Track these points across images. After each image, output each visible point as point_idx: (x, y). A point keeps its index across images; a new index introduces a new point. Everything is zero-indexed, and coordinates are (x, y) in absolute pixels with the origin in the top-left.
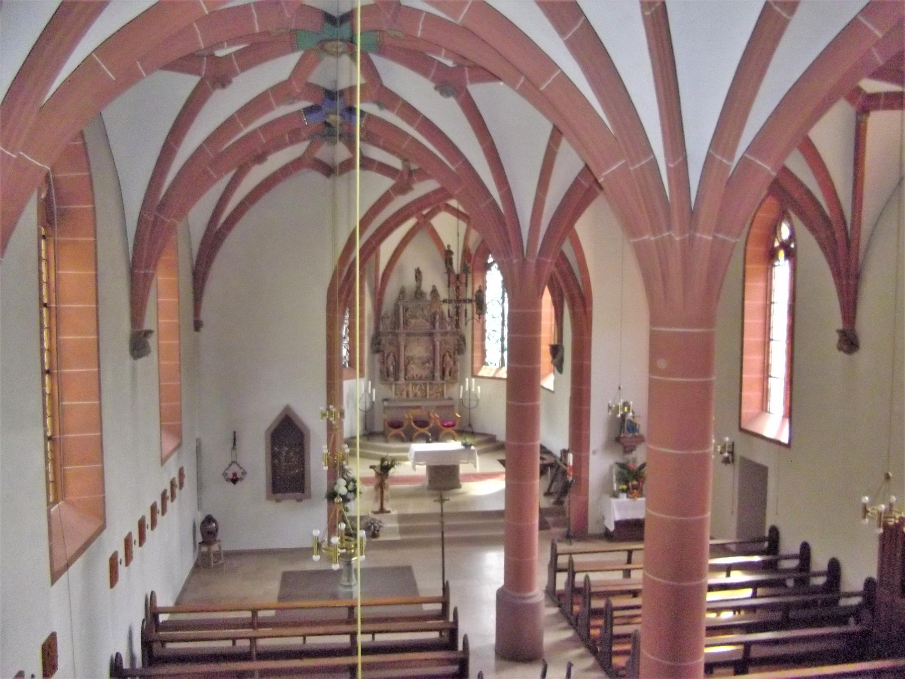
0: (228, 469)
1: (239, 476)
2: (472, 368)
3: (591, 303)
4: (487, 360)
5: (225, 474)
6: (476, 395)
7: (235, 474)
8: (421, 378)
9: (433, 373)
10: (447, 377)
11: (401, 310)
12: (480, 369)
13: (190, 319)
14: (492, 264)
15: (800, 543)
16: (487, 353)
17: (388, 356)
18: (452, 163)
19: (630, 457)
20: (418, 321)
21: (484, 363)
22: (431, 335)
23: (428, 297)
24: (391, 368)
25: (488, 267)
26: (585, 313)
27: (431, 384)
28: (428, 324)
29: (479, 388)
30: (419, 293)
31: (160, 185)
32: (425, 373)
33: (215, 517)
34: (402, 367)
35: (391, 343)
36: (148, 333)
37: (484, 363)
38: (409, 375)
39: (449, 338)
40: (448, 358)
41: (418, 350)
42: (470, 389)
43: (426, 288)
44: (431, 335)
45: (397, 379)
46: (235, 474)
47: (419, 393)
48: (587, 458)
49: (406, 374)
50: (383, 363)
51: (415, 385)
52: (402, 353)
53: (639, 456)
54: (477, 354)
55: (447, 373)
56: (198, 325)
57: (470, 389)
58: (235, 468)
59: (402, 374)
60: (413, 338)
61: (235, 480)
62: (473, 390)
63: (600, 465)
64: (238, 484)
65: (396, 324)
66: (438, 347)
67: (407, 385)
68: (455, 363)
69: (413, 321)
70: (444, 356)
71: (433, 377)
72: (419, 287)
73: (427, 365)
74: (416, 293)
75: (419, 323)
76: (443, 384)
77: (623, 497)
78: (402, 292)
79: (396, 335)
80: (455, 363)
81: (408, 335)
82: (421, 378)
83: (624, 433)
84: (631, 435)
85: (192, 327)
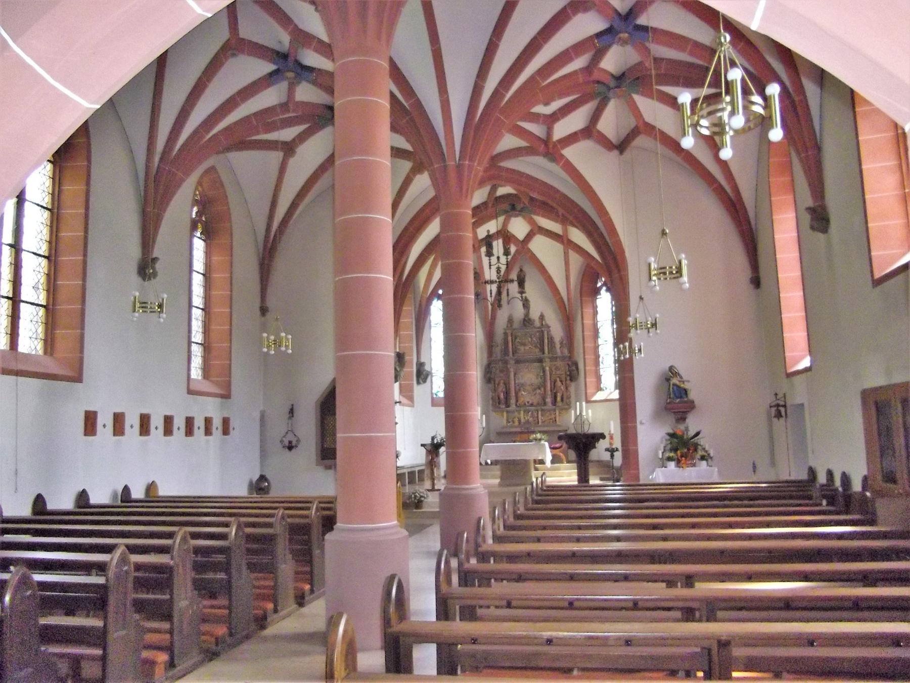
0: (284, 437)
1: (294, 444)
2: (586, 393)
3: (626, 269)
4: (602, 386)
5: (281, 441)
6: (587, 419)
7: (290, 442)
8: (532, 405)
9: (544, 399)
10: (559, 404)
11: (510, 338)
12: (594, 394)
13: (257, 304)
14: (601, 288)
15: (825, 471)
16: (602, 378)
17: (499, 384)
18: (407, 101)
19: (682, 427)
20: (527, 348)
21: (599, 389)
22: (540, 361)
23: (537, 324)
24: (502, 396)
25: (597, 292)
26: (621, 278)
27: (542, 410)
28: (537, 350)
29: (590, 411)
30: (527, 321)
31: (171, 149)
32: (535, 399)
33: (268, 477)
34: (513, 394)
35: (501, 371)
36: (154, 260)
37: (599, 389)
38: (520, 402)
39: (559, 363)
40: (559, 383)
41: (529, 376)
42: (581, 413)
43: (535, 314)
44: (540, 361)
45: (508, 405)
46: (290, 442)
47: (531, 419)
48: (635, 427)
49: (517, 401)
50: (495, 390)
51: (526, 412)
52: (512, 383)
53: (693, 424)
54: (591, 380)
55: (559, 399)
56: (264, 310)
57: (581, 413)
58: (290, 437)
59: (513, 401)
60: (522, 365)
61: (290, 447)
62: (584, 413)
63: (651, 437)
64: (294, 450)
65: (505, 352)
66: (548, 373)
67: (519, 412)
68: (567, 388)
69: (522, 348)
70: (555, 382)
71: (545, 404)
72: (527, 314)
73: (538, 391)
74: (524, 320)
75: (528, 349)
76: (555, 410)
77: (672, 465)
78: (510, 320)
79: (506, 362)
80: (567, 388)
81: (518, 362)
82: (532, 405)
83: (676, 400)
84: (678, 400)
85: (259, 313)
